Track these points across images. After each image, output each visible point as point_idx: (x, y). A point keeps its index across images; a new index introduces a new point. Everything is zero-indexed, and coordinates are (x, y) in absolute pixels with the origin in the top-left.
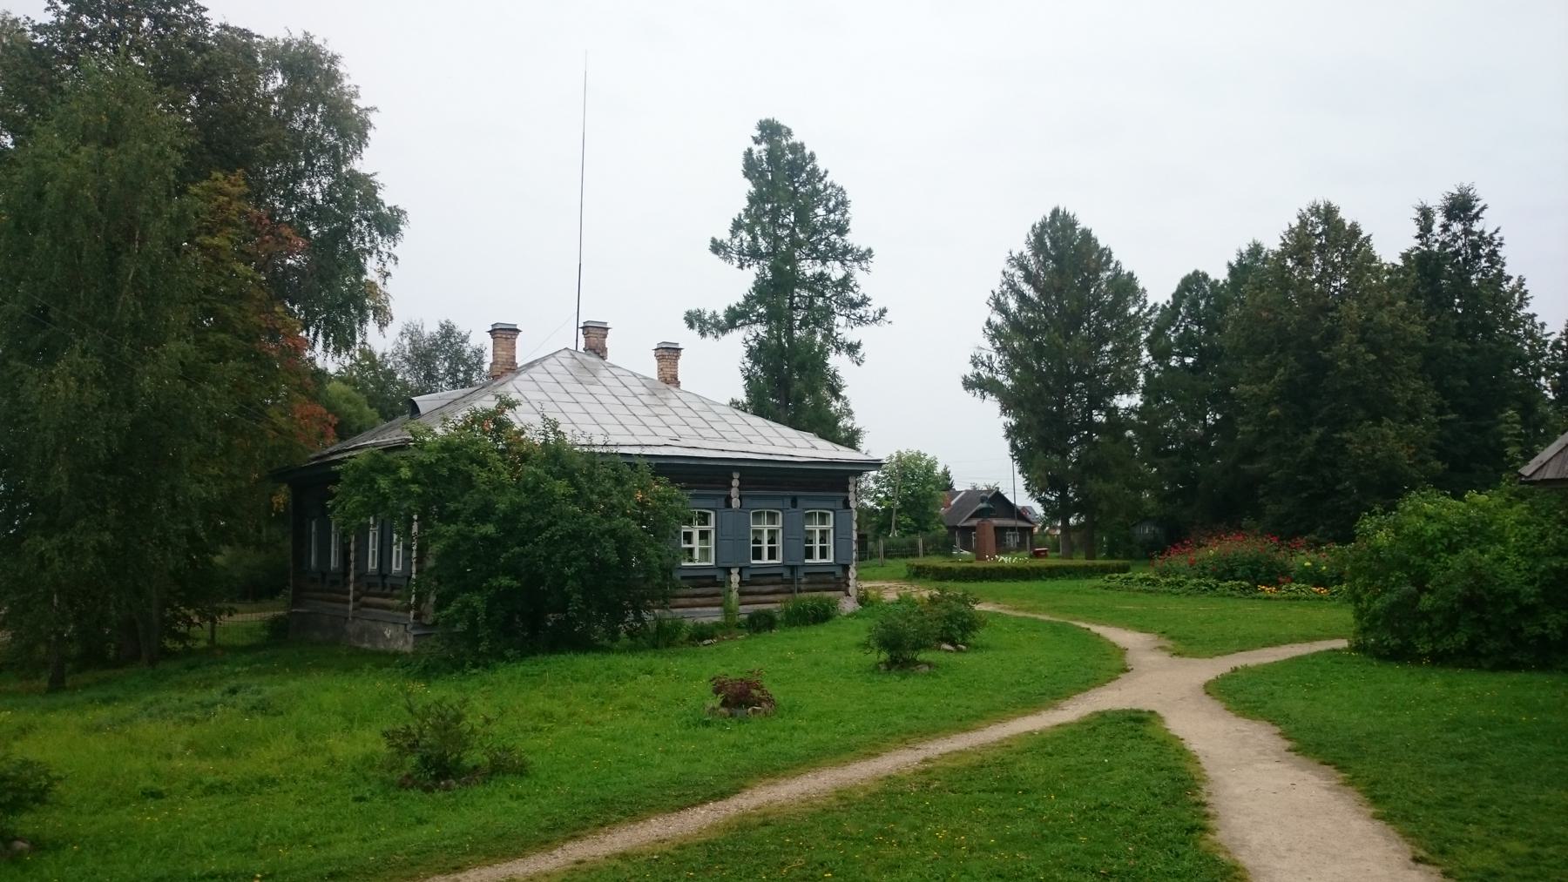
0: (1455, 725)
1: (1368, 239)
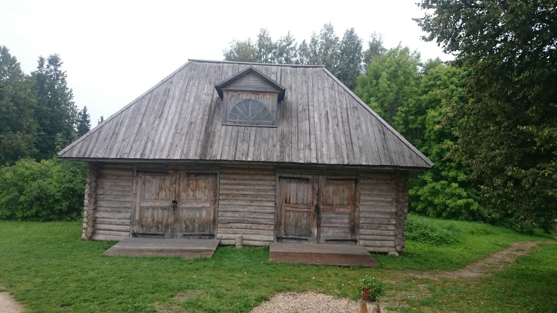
0: (25, 241)
1: (19, 64)
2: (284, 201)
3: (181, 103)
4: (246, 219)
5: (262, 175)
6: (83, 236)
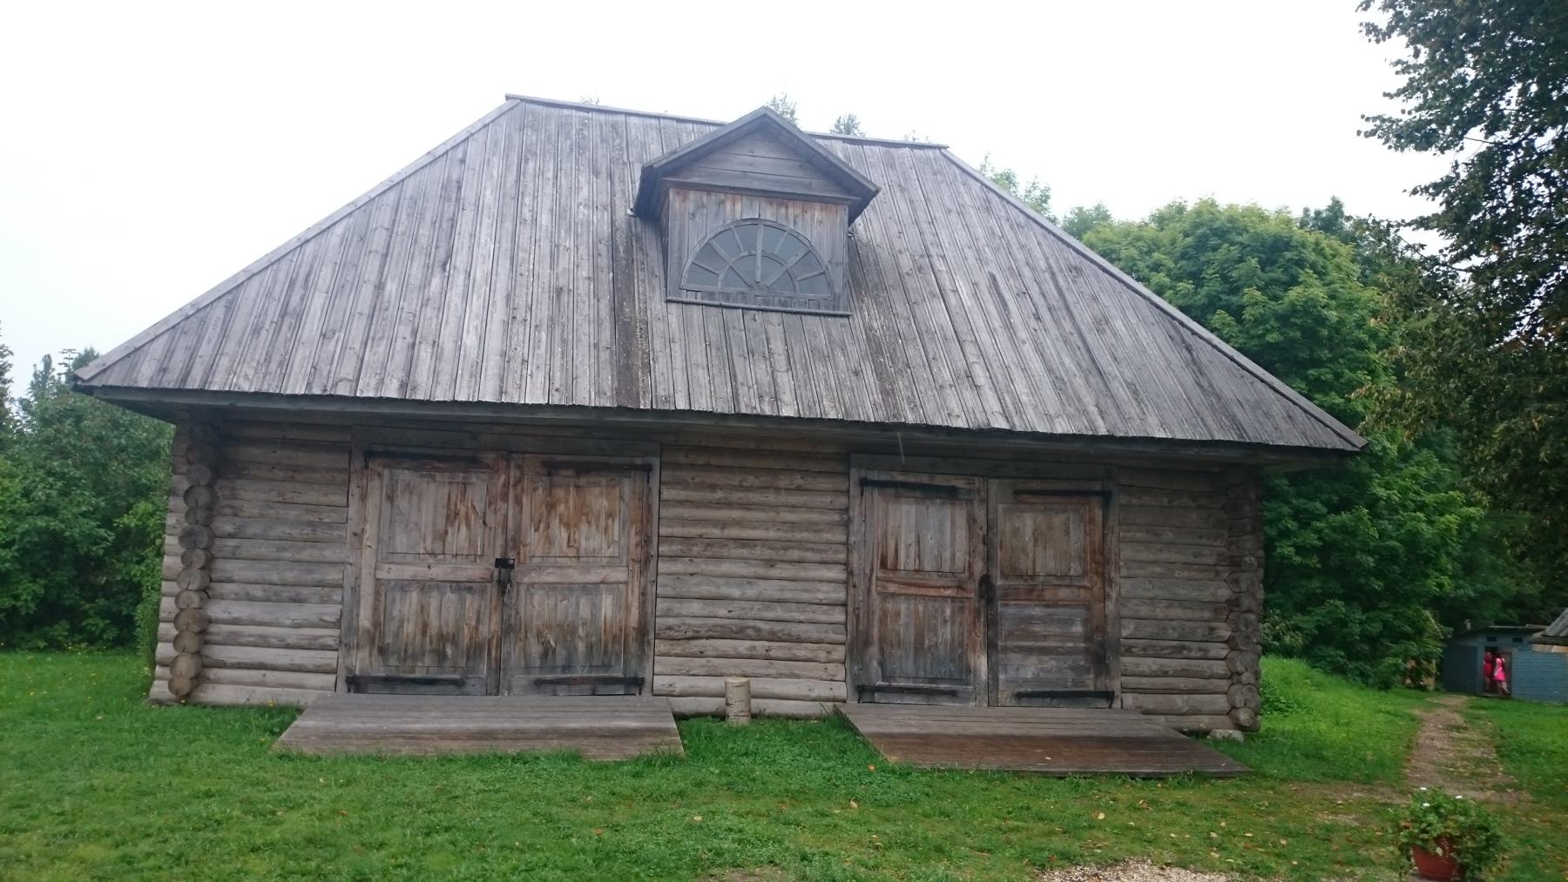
2: (877, 562)
3: (508, 226)
4: (751, 623)
5: (805, 473)
6: (160, 689)
